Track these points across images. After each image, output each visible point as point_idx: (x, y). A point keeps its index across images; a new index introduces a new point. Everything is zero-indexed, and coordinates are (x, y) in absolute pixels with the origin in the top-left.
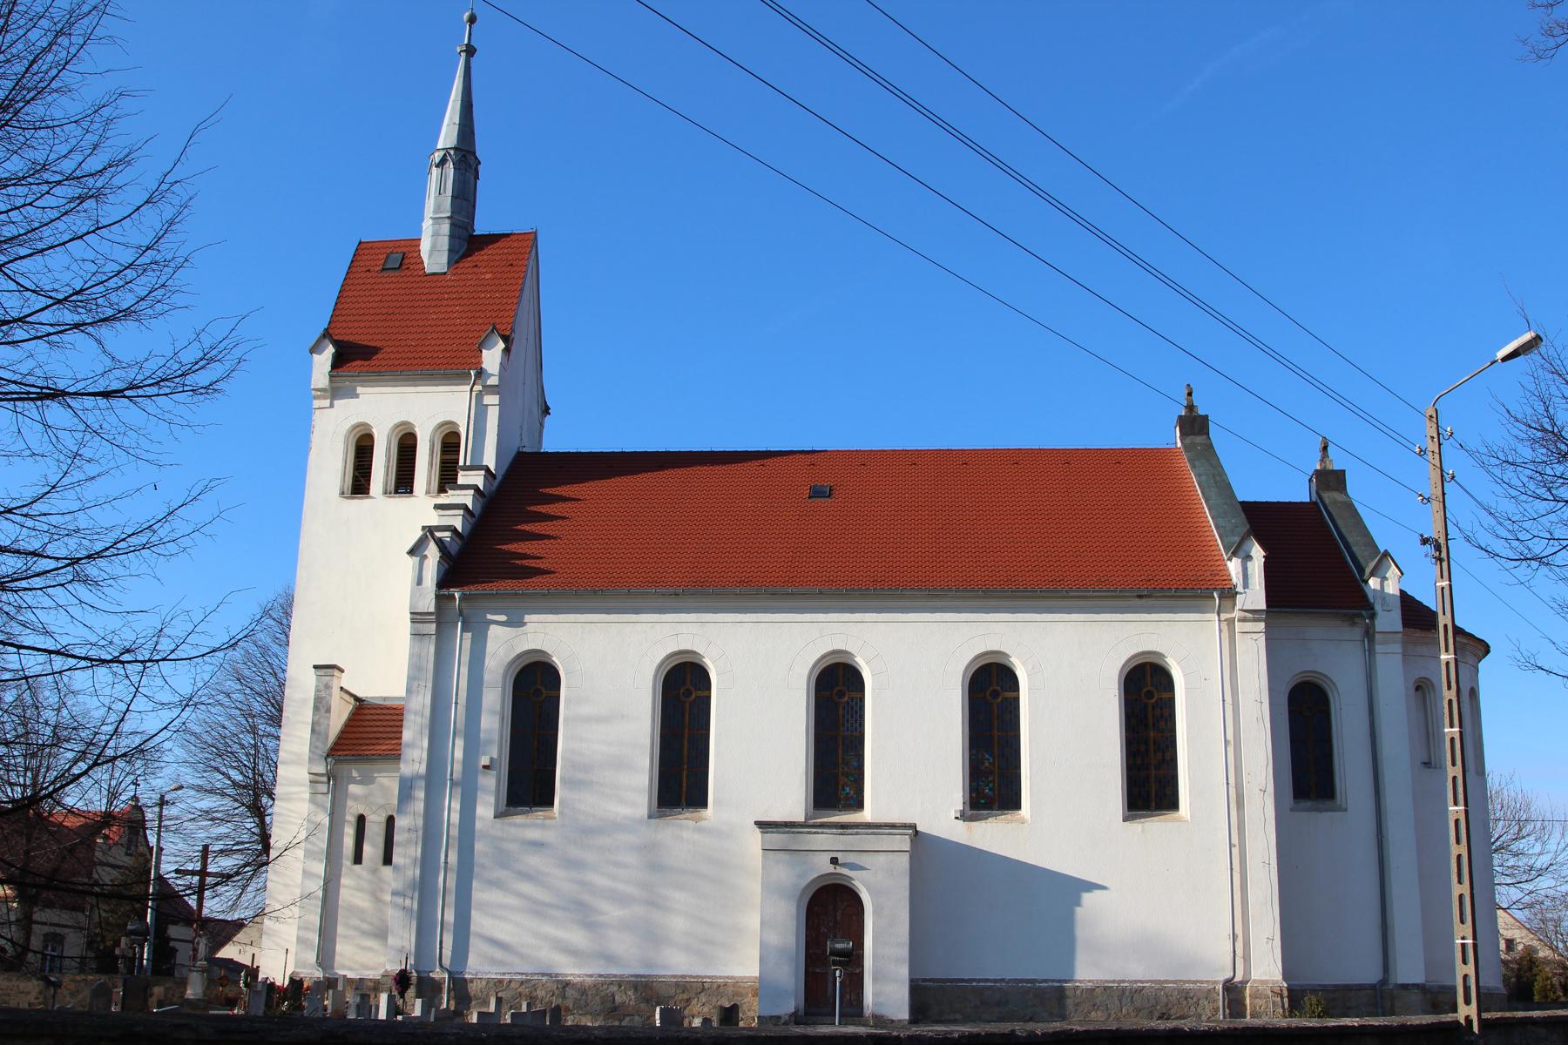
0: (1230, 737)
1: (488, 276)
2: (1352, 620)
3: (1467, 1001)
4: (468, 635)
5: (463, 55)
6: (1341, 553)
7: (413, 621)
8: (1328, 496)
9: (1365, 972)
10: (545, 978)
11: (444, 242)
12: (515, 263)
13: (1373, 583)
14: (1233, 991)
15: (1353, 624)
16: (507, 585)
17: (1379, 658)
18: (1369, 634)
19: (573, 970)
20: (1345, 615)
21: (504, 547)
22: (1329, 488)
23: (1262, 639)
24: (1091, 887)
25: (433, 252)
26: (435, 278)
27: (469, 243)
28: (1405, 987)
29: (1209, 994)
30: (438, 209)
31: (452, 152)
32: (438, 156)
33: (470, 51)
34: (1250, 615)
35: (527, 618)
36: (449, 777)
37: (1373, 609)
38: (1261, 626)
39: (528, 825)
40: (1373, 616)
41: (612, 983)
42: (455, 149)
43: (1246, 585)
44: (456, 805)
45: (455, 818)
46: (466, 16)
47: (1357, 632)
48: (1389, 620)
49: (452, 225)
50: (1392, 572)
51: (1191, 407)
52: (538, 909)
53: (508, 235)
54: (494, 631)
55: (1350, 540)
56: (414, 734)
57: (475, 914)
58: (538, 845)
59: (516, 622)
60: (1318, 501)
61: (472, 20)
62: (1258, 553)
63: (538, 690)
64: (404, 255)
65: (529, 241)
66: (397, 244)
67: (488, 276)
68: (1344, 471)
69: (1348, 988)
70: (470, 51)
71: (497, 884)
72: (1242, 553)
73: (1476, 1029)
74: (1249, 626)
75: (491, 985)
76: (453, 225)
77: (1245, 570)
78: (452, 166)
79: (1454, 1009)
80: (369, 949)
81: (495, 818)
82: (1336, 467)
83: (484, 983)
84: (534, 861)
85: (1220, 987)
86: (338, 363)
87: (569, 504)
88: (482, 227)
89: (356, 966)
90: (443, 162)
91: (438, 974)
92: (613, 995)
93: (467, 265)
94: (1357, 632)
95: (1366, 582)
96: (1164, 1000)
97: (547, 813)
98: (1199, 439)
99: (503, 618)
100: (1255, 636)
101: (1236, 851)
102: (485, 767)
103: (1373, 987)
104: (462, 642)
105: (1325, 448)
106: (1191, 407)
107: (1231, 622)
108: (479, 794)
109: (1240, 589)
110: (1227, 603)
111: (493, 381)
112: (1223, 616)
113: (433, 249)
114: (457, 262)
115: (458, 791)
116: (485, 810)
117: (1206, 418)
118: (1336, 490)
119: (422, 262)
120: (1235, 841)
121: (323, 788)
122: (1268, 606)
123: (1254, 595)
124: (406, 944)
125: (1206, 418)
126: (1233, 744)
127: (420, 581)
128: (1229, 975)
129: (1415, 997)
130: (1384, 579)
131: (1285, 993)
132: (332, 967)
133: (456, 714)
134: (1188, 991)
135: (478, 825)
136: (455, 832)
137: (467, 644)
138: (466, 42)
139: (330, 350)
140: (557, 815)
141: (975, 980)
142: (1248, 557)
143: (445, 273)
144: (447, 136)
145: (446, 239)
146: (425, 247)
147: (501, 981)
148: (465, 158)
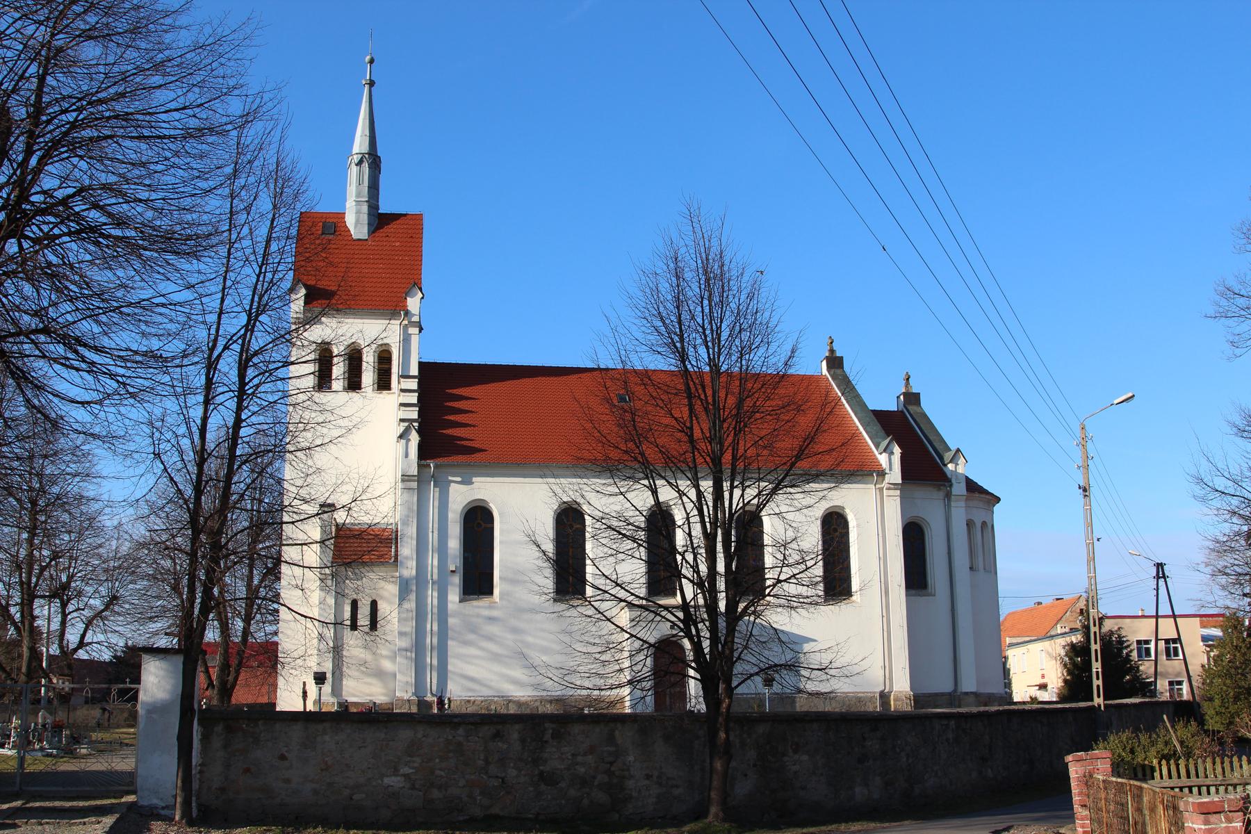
0: (881, 556)
1: (397, 244)
2: (939, 488)
3: (1099, 696)
4: (437, 489)
5: (367, 86)
6: (924, 445)
7: (403, 481)
8: (912, 408)
9: (947, 687)
10: (496, 699)
11: (365, 218)
12: (414, 235)
13: (951, 466)
14: (884, 696)
15: (939, 490)
16: (460, 458)
17: (953, 509)
18: (948, 495)
19: (522, 693)
20: (935, 485)
21: (444, 432)
22: (910, 404)
23: (898, 499)
24: (808, 640)
25: (356, 223)
26: (361, 243)
27: (379, 219)
28: (966, 693)
29: (872, 699)
30: (358, 195)
31: (367, 156)
32: (356, 158)
33: (372, 84)
34: (892, 486)
35: (474, 479)
36: (429, 577)
37: (951, 481)
38: (898, 492)
39: (479, 606)
40: (951, 486)
41: (536, 700)
42: (369, 154)
43: (891, 469)
44: (435, 594)
45: (435, 602)
46: (368, 59)
47: (941, 494)
48: (959, 489)
49: (369, 206)
50: (962, 460)
51: (832, 351)
52: (496, 657)
53: (405, 215)
54: (453, 487)
55: (931, 438)
56: (407, 550)
57: (450, 660)
58: (491, 619)
59: (467, 482)
60: (905, 410)
61: (372, 61)
62: (897, 450)
63: (479, 523)
64: (333, 225)
65: (417, 219)
66: (328, 215)
67: (397, 244)
68: (842, 357)
69: (936, 695)
70: (372, 84)
71: (466, 643)
72: (888, 451)
73: (1102, 708)
74: (892, 492)
75: (463, 703)
76: (369, 207)
77: (890, 460)
78: (367, 165)
79: (1092, 700)
80: (370, 684)
81: (460, 602)
82: (914, 391)
83: (458, 702)
84: (493, 629)
85: (878, 695)
86: (309, 300)
87: (470, 402)
88: (384, 208)
89: (358, 694)
90: (360, 163)
91: (429, 698)
92: (537, 708)
93: (381, 235)
94: (941, 494)
95: (945, 465)
96: (848, 703)
97: (490, 599)
98: (839, 371)
99: (459, 479)
100: (895, 498)
101: (885, 619)
102: (452, 571)
103: (950, 694)
104: (433, 493)
105: (908, 379)
106: (832, 351)
107: (881, 490)
108: (449, 587)
109: (887, 471)
110: (880, 478)
111: (416, 319)
112: (878, 486)
113: (357, 222)
114: (373, 232)
115: (436, 587)
116: (454, 596)
117: (841, 358)
118: (914, 404)
119: (349, 231)
120: (884, 614)
121: (329, 582)
122: (903, 478)
123: (895, 475)
124: (409, 680)
125: (841, 358)
126: (883, 559)
127: (407, 456)
128: (882, 688)
129: (971, 699)
130: (957, 464)
131: (912, 698)
132: (341, 695)
133: (433, 538)
134: (860, 698)
135: (450, 606)
136: (435, 610)
137: (437, 495)
138: (368, 78)
139: (303, 291)
140: (498, 600)
141: (744, 694)
142: (892, 453)
143: (367, 240)
144: (360, 144)
145: (366, 217)
146: (350, 220)
147: (469, 701)
148: (373, 160)
